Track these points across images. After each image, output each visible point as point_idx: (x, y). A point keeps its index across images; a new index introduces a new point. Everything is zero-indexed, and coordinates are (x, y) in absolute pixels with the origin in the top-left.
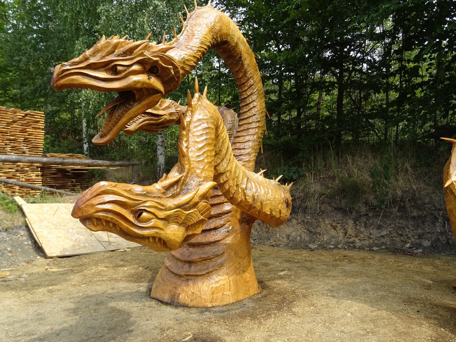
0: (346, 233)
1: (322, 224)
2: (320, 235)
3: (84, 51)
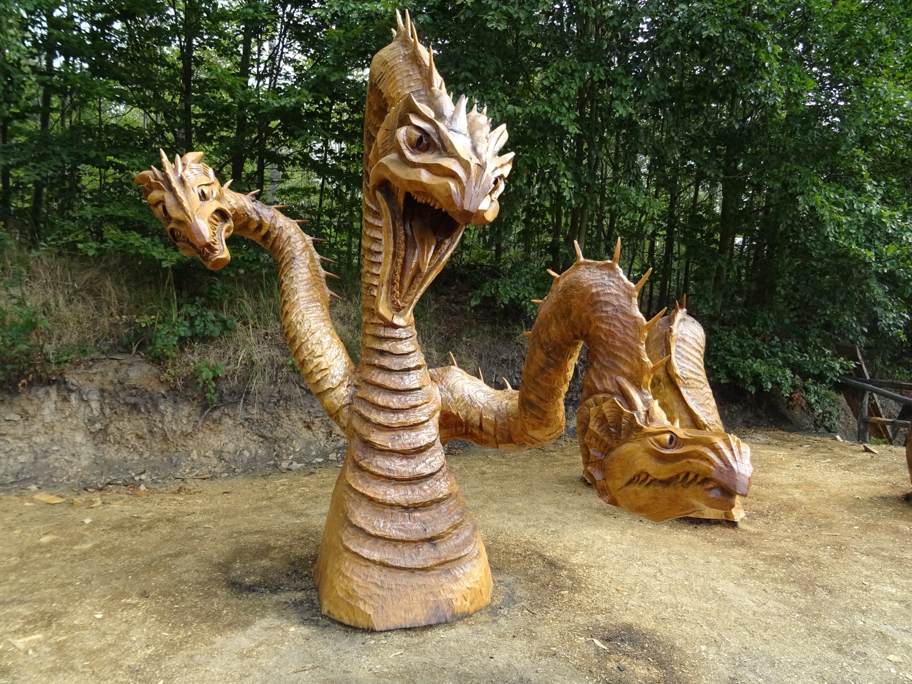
0: (331, 432)
1: (286, 423)
2: (285, 441)
3: (674, 115)
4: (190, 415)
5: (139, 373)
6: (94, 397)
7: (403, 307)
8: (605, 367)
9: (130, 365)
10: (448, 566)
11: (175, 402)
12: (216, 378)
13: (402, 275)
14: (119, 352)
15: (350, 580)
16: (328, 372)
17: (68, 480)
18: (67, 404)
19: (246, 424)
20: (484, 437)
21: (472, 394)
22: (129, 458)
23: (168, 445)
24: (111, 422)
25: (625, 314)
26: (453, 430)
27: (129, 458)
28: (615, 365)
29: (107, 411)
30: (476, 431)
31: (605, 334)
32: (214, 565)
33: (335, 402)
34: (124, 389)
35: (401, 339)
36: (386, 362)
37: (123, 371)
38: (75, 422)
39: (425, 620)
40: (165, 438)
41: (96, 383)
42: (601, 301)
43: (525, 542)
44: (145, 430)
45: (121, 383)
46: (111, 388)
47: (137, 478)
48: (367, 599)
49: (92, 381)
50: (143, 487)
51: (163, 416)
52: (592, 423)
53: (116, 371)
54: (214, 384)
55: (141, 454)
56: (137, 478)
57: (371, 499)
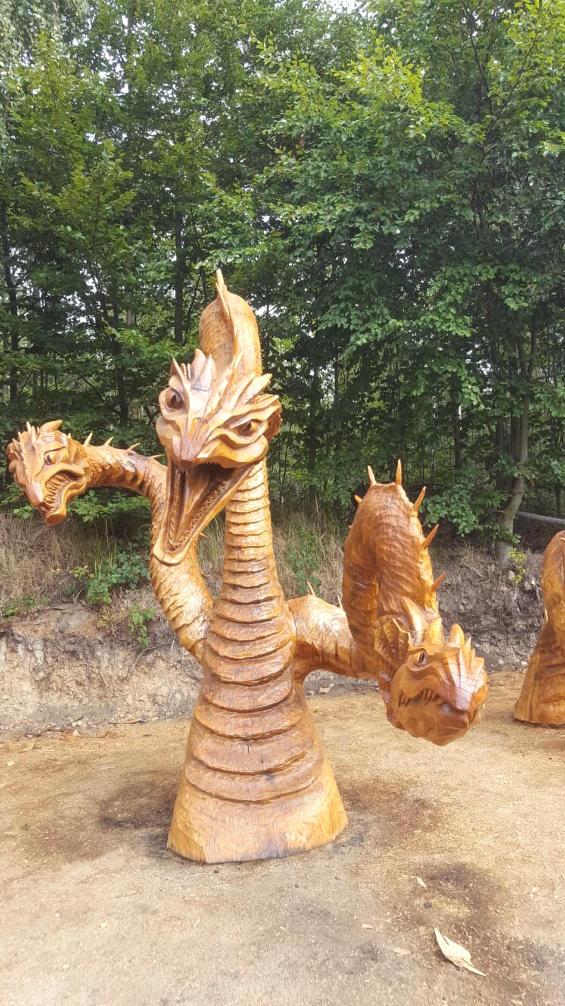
4: (125, 660)
5: (78, 620)
6: (39, 646)
7: (177, 547)
8: (390, 588)
9: (71, 614)
10: (283, 798)
11: (112, 647)
12: (148, 622)
13: (179, 518)
14: (63, 602)
15: (188, 812)
16: (183, 609)
17: (14, 727)
18: (15, 655)
19: (179, 666)
20: (341, 667)
21: (329, 625)
22: (70, 705)
23: (104, 690)
24: (54, 670)
25: (403, 534)
26: (311, 660)
27: (70, 705)
28: (397, 585)
29: (50, 659)
30: (332, 661)
31: (387, 556)
32: (97, 803)
33: (190, 637)
34: (64, 638)
35: (253, 573)
36: (237, 596)
37: (64, 619)
38: (22, 671)
39: (257, 854)
40: (102, 685)
41: (40, 633)
42: (382, 524)
43: (407, 781)
44: (84, 677)
45: (61, 632)
46: (52, 637)
47: (74, 724)
48: (201, 831)
49: (36, 632)
50: (76, 733)
51: (99, 662)
52: (377, 645)
53: (58, 621)
54: (145, 628)
55: (81, 701)
56: (74, 724)
57: (212, 732)
